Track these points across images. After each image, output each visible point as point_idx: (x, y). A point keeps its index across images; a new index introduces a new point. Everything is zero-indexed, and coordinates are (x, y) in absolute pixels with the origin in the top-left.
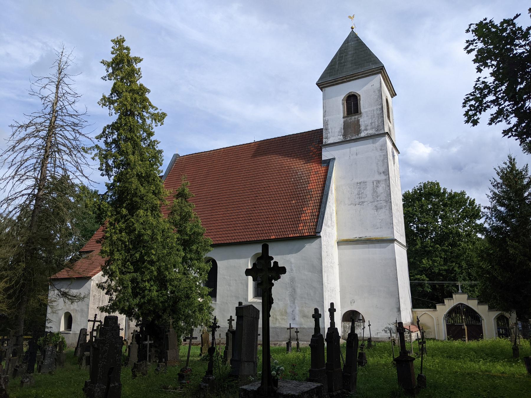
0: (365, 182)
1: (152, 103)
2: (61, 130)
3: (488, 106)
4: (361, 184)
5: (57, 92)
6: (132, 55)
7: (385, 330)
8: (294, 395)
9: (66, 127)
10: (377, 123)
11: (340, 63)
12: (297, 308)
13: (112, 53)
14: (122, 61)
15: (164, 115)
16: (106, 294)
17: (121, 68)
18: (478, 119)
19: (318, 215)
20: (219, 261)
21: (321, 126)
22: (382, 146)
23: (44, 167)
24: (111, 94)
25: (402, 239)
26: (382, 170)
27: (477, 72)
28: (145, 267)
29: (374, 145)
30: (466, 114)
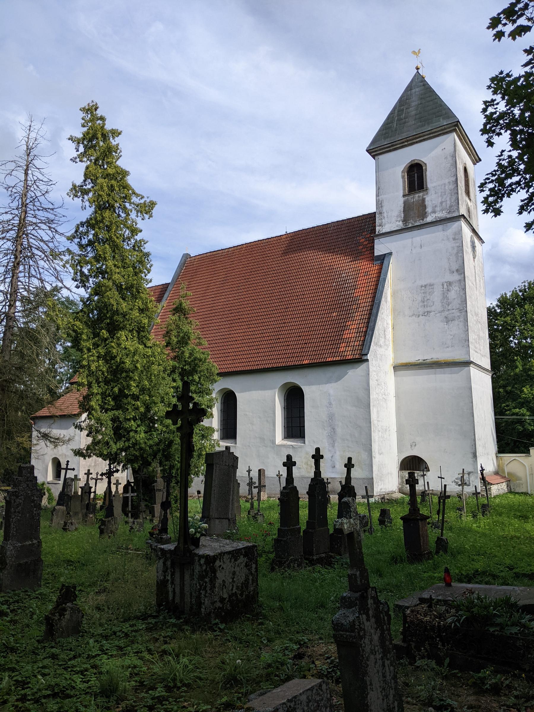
0: (431, 285)
1: (137, 191)
2: (34, 229)
3: (513, 190)
4: (427, 288)
5: (26, 180)
6: (108, 127)
7: (455, 482)
8: (208, 555)
9: (39, 225)
10: (448, 202)
11: (399, 120)
12: (338, 453)
13: (83, 126)
14: (95, 137)
15: (152, 204)
16: (88, 436)
17: (95, 146)
18: (501, 206)
19: (366, 331)
20: (238, 393)
21: (372, 209)
22: (455, 234)
23: (15, 277)
24: (85, 181)
25: (486, 363)
26: (455, 267)
27: (488, 146)
28: (129, 403)
29: (445, 233)
30: (485, 201)
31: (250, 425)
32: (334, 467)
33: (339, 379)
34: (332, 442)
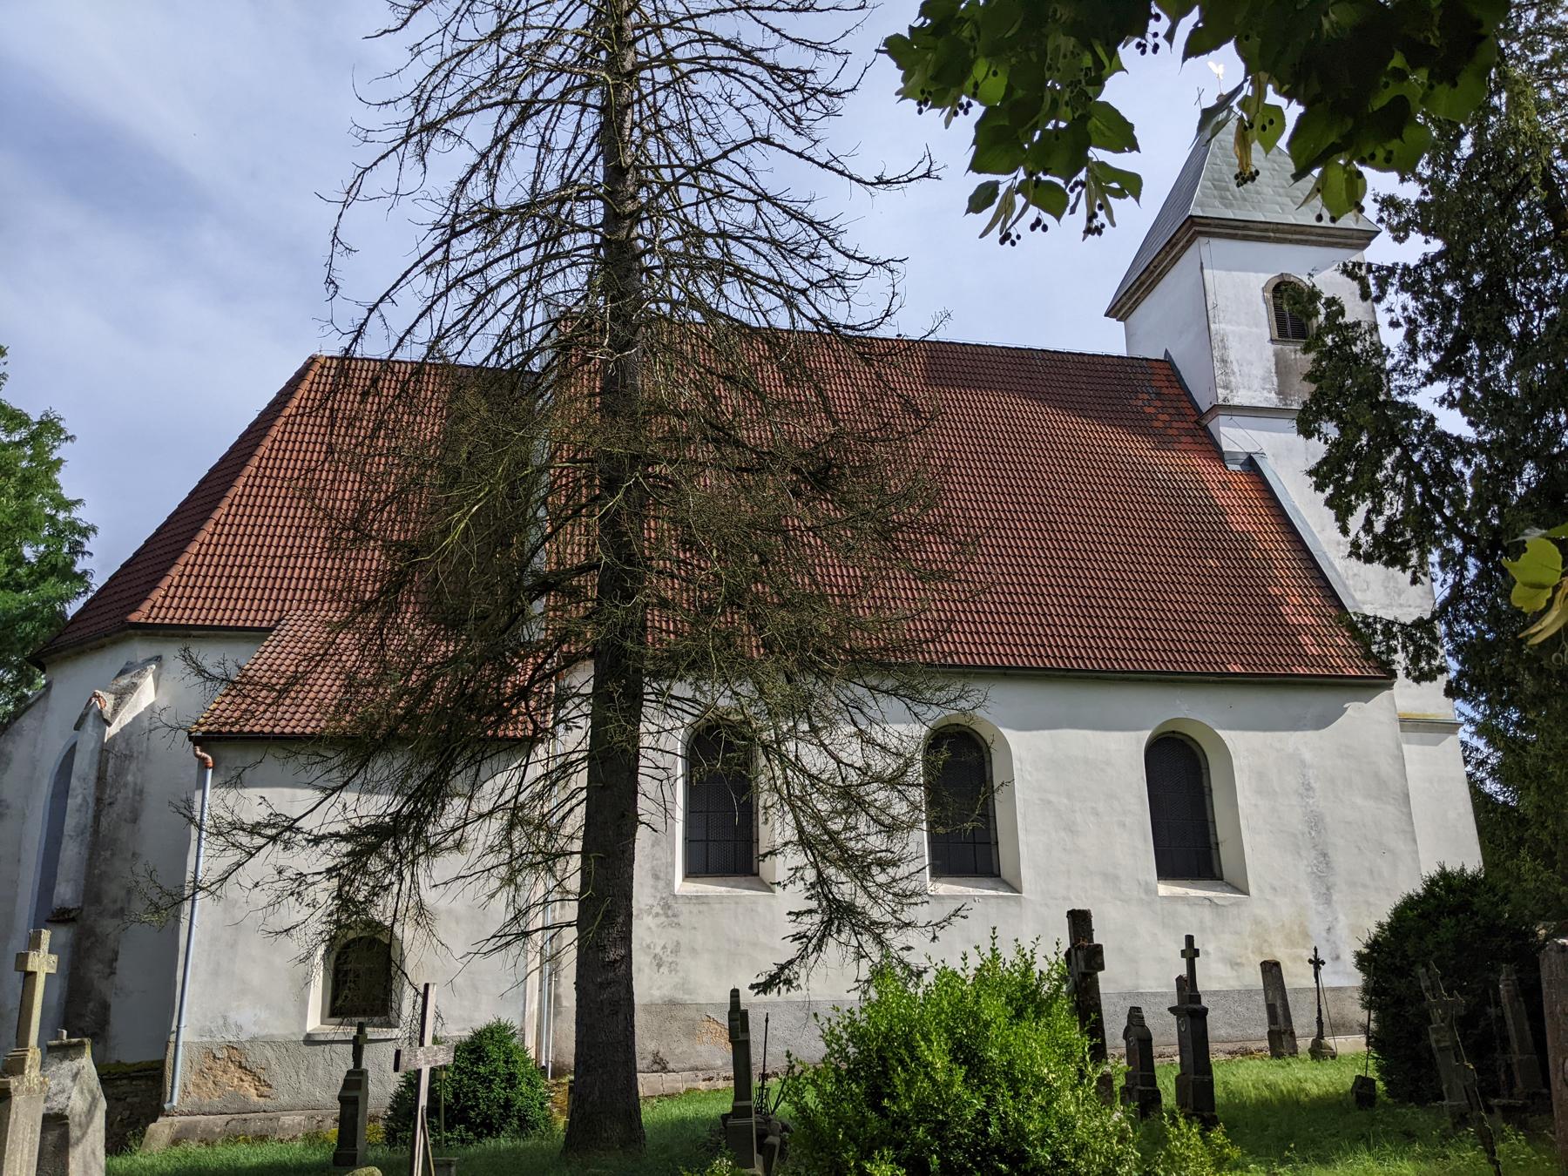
31: (1063, 834)
32: (1338, 958)
33: (1322, 722)
34: (1324, 890)
